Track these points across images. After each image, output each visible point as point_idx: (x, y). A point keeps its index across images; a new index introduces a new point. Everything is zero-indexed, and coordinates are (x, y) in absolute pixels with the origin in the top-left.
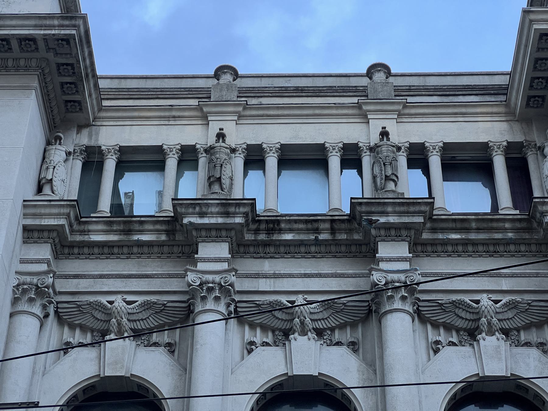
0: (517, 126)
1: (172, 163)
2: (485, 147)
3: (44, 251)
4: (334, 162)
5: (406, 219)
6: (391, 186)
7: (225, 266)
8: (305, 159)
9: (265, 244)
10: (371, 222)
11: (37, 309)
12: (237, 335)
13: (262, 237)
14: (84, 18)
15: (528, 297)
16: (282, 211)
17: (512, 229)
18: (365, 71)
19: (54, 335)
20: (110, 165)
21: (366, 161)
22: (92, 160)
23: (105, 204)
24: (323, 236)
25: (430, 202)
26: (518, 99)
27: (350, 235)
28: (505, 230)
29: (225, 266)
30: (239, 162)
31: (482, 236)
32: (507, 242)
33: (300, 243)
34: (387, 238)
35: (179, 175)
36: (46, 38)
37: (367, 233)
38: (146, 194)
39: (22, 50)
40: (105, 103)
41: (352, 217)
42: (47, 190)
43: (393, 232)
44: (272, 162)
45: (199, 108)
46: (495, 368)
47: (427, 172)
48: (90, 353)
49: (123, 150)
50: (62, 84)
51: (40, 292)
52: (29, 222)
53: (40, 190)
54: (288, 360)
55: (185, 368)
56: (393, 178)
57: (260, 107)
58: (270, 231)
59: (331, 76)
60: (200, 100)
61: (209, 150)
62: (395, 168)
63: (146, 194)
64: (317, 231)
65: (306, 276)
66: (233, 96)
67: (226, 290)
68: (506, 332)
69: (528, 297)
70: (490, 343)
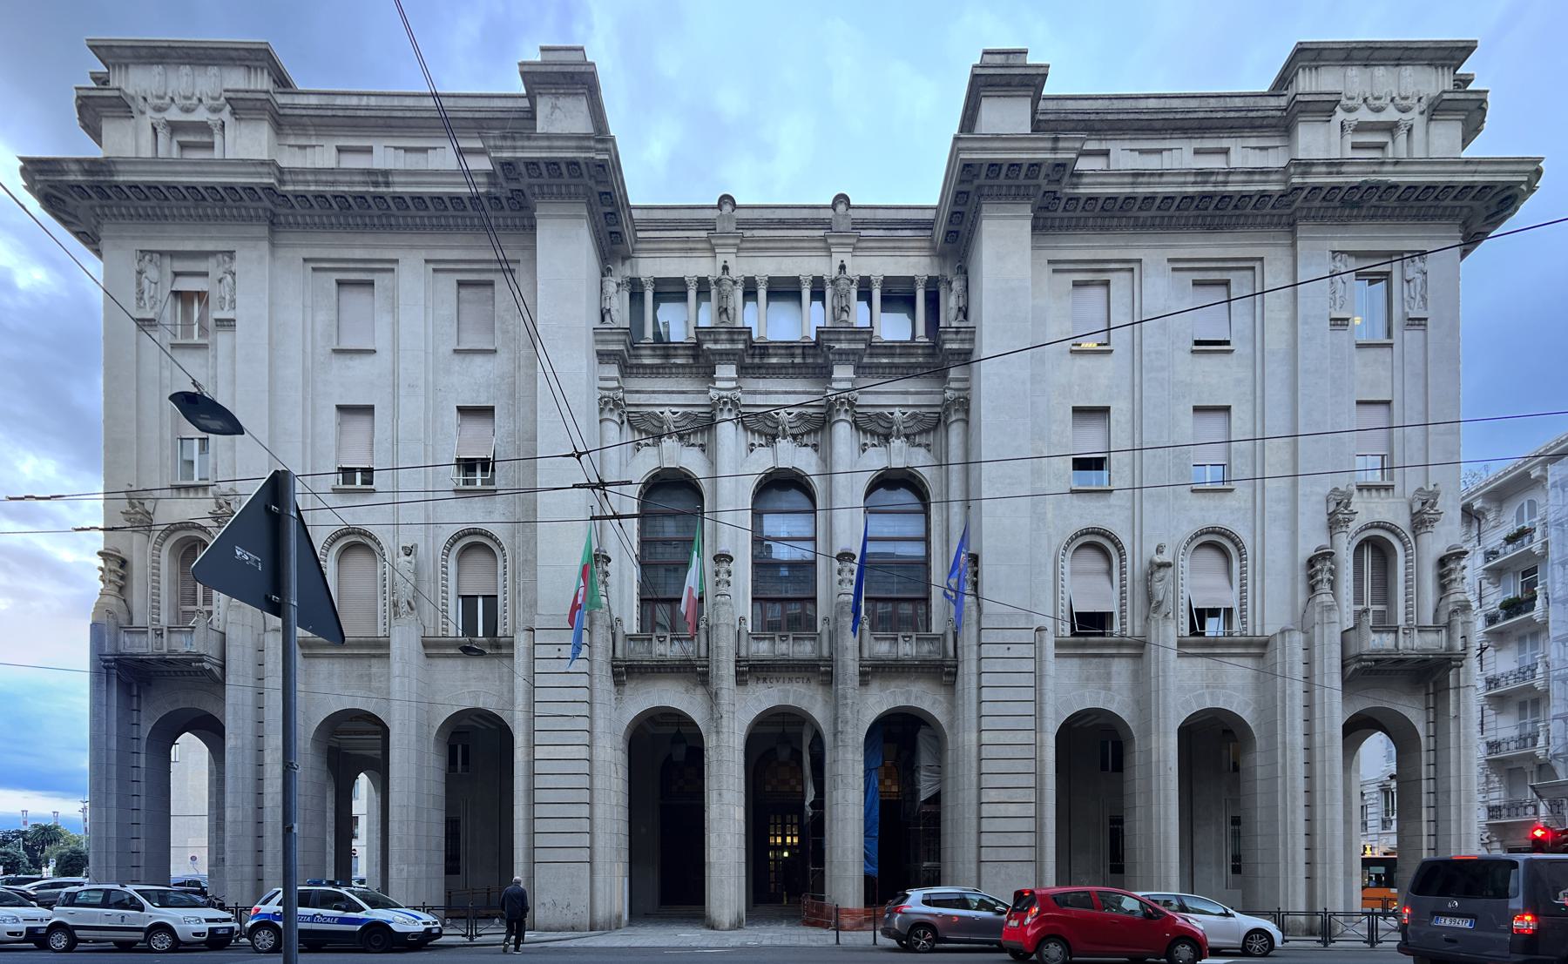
0: (936, 260)
1: (692, 294)
2: (911, 280)
3: (613, 370)
4: (806, 294)
5: (853, 346)
6: (844, 316)
7: (734, 384)
8: (784, 291)
9: (760, 367)
10: (830, 348)
11: (616, 418)
12: (745, 439)
13: (757, 360)
14: (612, 140)
15: (924, 410)
16: (770, 338)
17: (924, 355)
18: (830, 203)
19: (629, 436)
20: (649, 296)
21: (829, 293)
22: (635, 290)
23: (649, 333)
24: (798, 360)
25: (869, 331)
26: (939, 232)
27: (811, 360)
28: (916, 355)
29: (734, 384)
30: (739, 293)
31: (903, 360)
32: (919, 365)
33: (783, 366)
34: (841, 362)
35: (698, 307)
36: (588, 161)
37: (826, 357)
38: (678, 322)
39: (571, 176)
40: (640, 234)
41: (817, 344)
42: (608, 319)
43: (844, 356)
44: (762, 293)
45: (708, 240)
46: (898, 463)
47: (870, 305)
48: (652, 451)
49: (657, 282)
50: (606, 214)
51: (617, 404)
52: (600, 347)
53: (603, 319)
54: (660, 454)
55: (826, 459)
56: (845, 310)
57: (753, 239)
58: (762, 356)
59: (804, 207)
60: (180, 266)
61: (718, 282)
62: (848, 300)
63: (678, 322)
64: (793, 355)
65: (786, 393)
66: (732, 227)
67: (735, 404)
68: (907, 436)
69: (924, 410)
70: (784, 445)
